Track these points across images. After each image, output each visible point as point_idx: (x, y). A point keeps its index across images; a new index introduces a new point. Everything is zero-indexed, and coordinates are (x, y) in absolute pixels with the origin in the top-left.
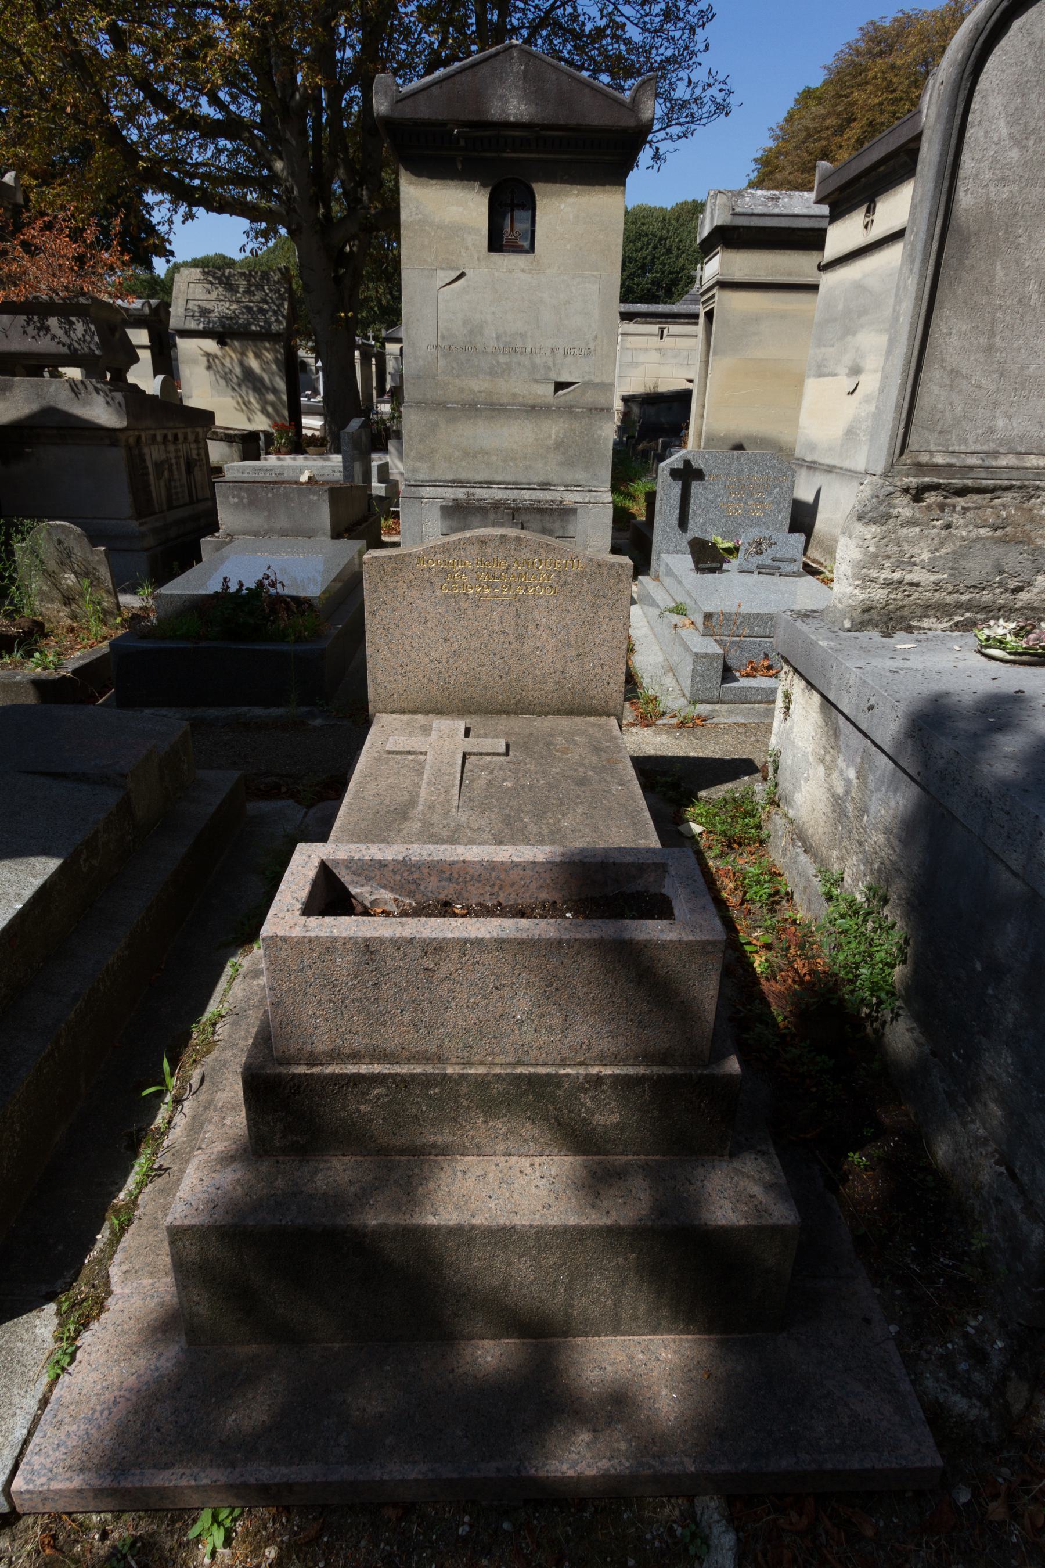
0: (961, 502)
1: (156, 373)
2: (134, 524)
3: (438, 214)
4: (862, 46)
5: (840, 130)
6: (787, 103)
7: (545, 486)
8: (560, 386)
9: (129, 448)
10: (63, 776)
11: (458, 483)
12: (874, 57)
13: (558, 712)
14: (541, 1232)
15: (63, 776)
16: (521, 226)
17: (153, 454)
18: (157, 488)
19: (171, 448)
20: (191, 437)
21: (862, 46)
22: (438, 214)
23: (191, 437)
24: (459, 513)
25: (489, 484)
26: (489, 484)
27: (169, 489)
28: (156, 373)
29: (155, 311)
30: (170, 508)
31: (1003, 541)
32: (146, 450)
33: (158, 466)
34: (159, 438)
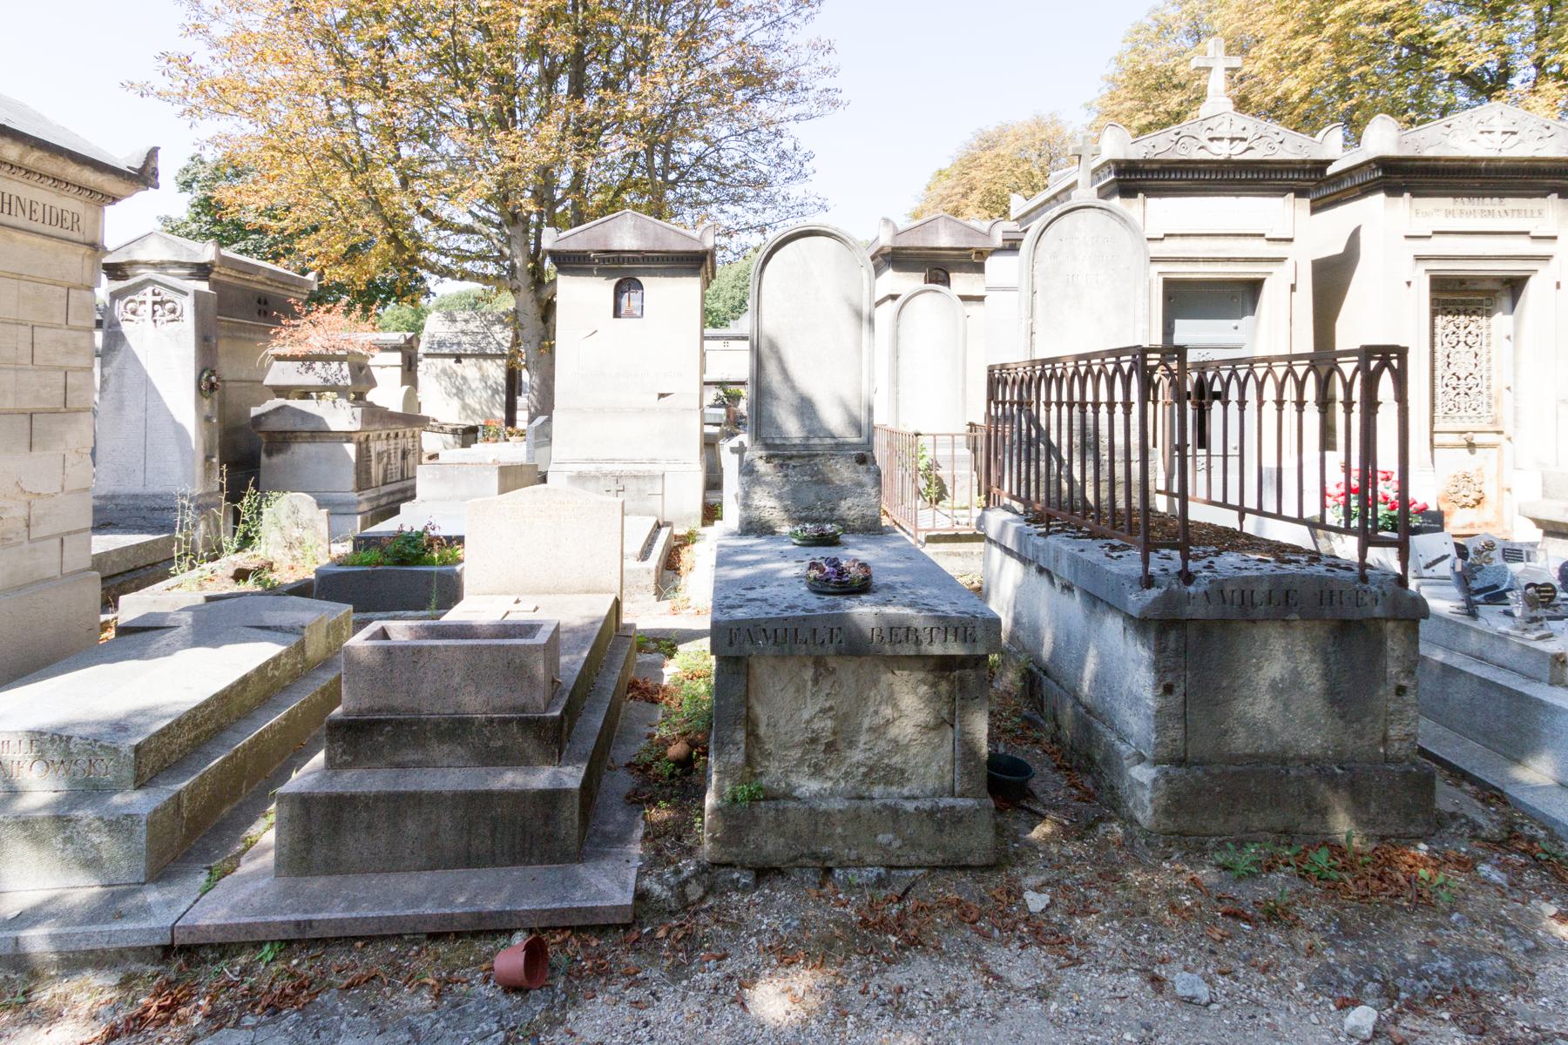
0: (792, 463)
1: (403, 384)
2: (354, 496)
3: (581, 299)
4: (975, 143)
5: (964, 195)
6: (926, 177)
7: (653, 461)
8: (662, 396)
9: (359, 444)
10: (268, 628)
11: (592, 461)
12: (984, 150)
13: (580, 592)
14: (455, 794)
15: (268, 628)
16: (635, 303)
17: (376, 447)
18: (376, 471)
19: (392, 442)
20: (409, 434)
21: (975, 143)
22: (581, 299)
23: (409, 434)
24: (580, 478)
25: (613, 461)
26: (613, 461)
27: (385, 471)
28: (403, 384)
29: (409, 341)
30: (385, 483)
31: (816, 483)
32: (372, 445)
33: (379, 454)
34: (384, 436)
